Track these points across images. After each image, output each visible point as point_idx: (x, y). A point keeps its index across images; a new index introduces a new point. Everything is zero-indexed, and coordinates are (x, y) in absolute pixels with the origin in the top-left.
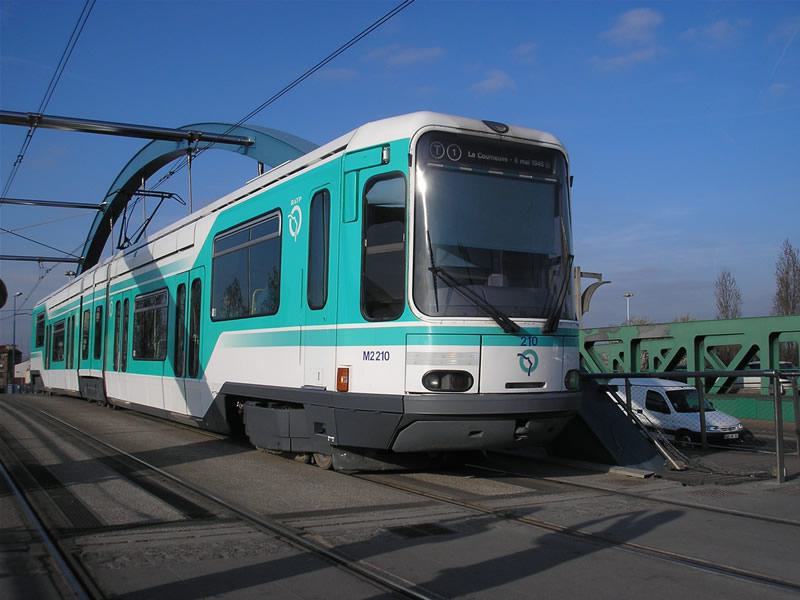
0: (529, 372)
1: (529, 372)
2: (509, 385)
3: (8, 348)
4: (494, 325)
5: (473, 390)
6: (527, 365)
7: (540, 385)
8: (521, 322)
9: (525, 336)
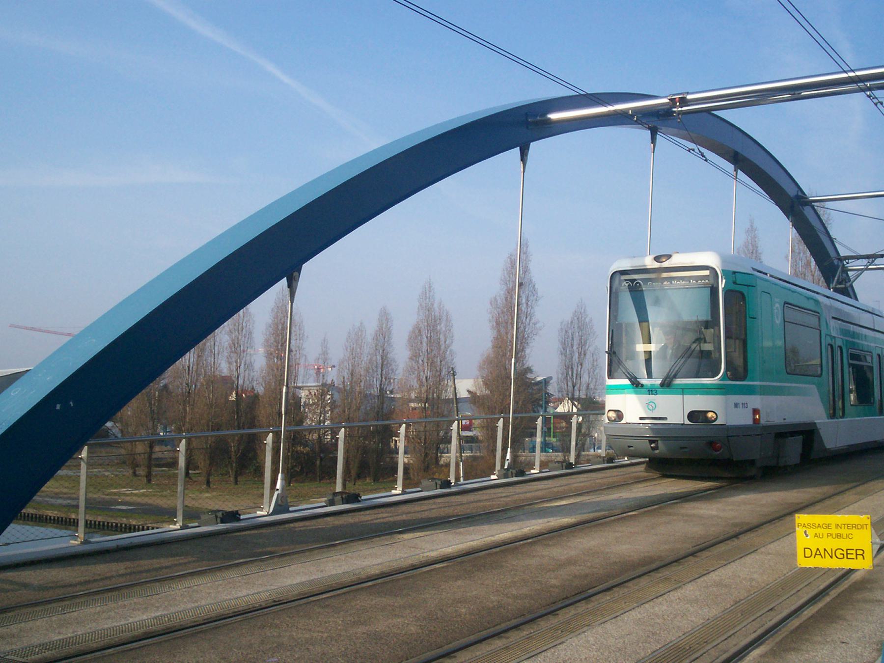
2: (641, 418)
7: (665, 419)
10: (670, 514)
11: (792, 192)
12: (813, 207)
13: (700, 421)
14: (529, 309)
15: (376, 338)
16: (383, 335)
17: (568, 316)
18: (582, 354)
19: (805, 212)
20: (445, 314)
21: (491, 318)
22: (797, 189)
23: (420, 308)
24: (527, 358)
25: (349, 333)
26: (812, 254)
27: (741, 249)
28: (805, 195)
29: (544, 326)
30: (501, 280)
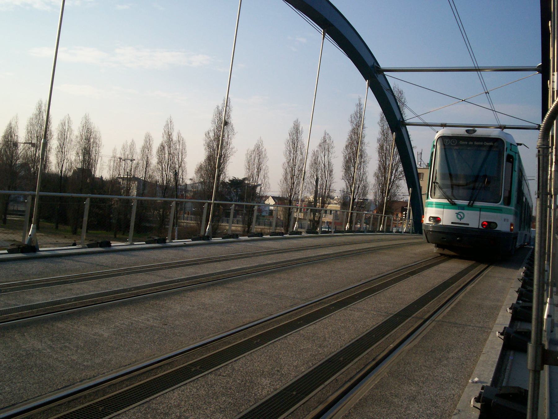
0: (460, 219)
1: (460, 219)
2: (452, 223)
4: (448, 202)
5: (441, 224)
6: (459, 217)
7: (468, 224)
8: (457, 202)
9: (462, 208)
10: (532, 206)
11: (370, 63)
12: (384, 75)
13: (234, 205)
14: (229, 140)
15: (143, 151)
16: (133, 145)
17: (252, 148)
18: (259, 170)
19: (378, 78)
20: (181, 139)
21: (205, 144)
22: (374, 61)
23: (164, 133)
24: (225, 169)
25: (124, 145)
26: (384, 115)
27: (353, 116)
28: (379, 66)
29: (237, 150)
30: (212, 121)
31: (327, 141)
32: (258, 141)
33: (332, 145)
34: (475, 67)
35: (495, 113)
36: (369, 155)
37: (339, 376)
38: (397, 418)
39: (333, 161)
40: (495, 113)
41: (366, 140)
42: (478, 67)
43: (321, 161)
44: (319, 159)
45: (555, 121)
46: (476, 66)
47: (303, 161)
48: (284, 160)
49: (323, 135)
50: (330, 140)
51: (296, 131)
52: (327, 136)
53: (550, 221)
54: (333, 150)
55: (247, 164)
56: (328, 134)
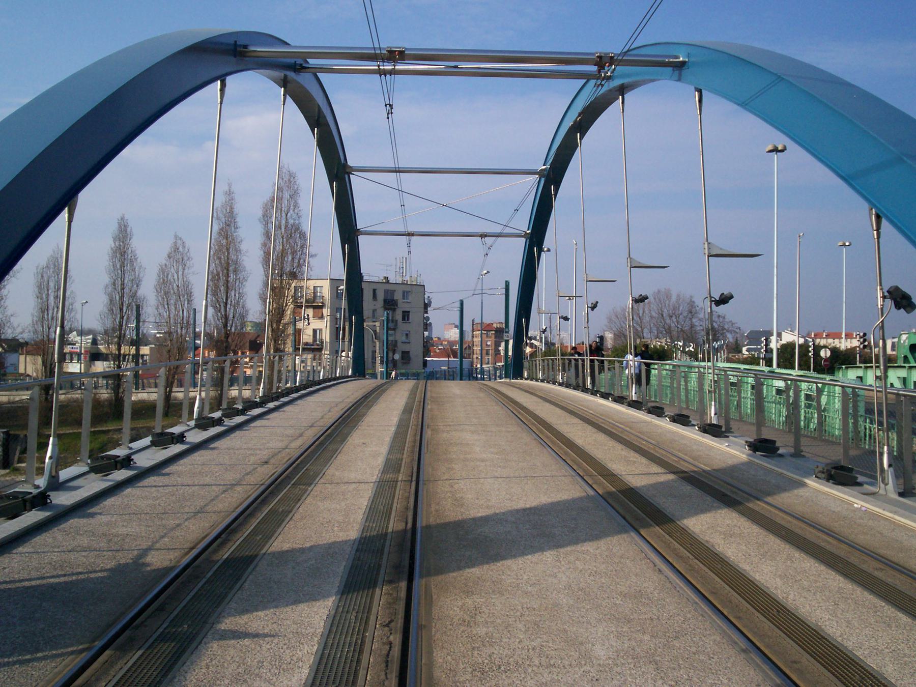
3: (495, 325)
29: (22, 269)
31: (181, 249)
32: (54, 252)
33: (188, 254)
34: (374, 49)
35: (400, 187)
36: (248, 268)
37: (128, 661)
38: (288, 686)
39: (192, 279)
40: (400, 187)
41: (244, 247)
42: (380, 49)
43: (172, 280)
44: (170, 276)
45: (552, 187)
46: (377, 46)
47: (137, 282)
48: (106, 279)
49: (172, 240)
50: (185, 247)
51: (123, 234)
52: (179, 242)
53: (631, 344)
54: (191, 262)
55: (36, 290)
56: (180, 239)
